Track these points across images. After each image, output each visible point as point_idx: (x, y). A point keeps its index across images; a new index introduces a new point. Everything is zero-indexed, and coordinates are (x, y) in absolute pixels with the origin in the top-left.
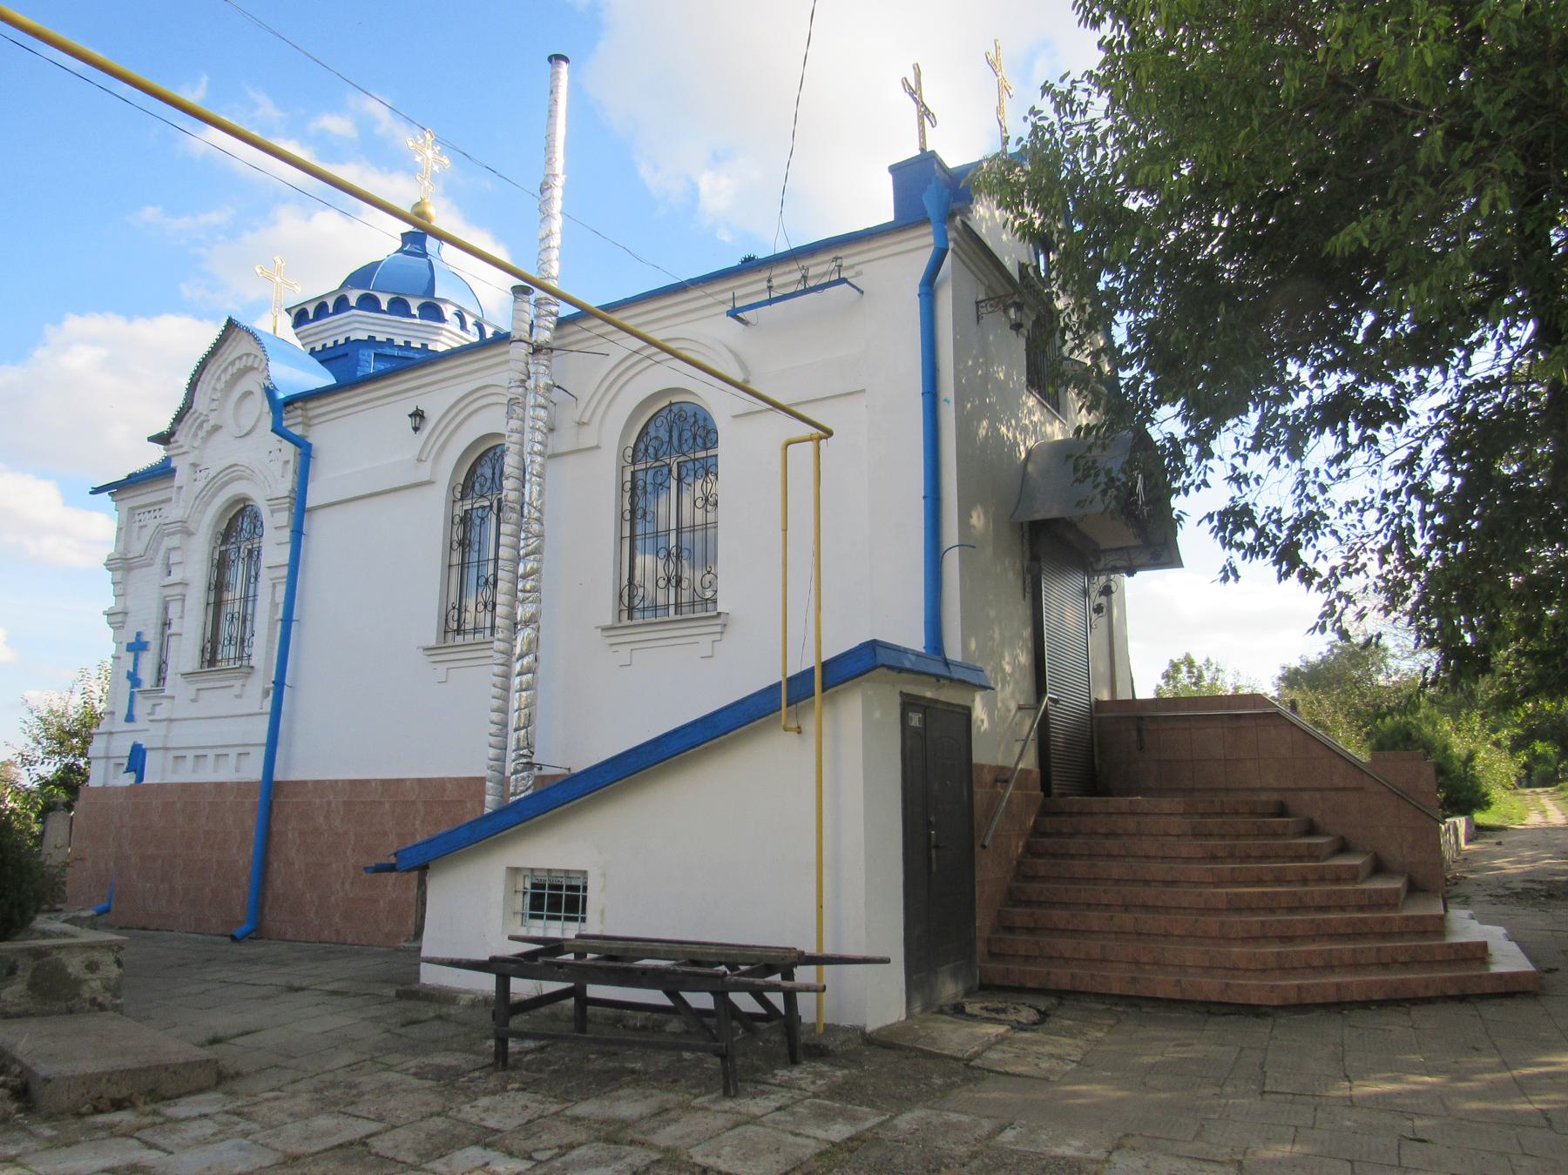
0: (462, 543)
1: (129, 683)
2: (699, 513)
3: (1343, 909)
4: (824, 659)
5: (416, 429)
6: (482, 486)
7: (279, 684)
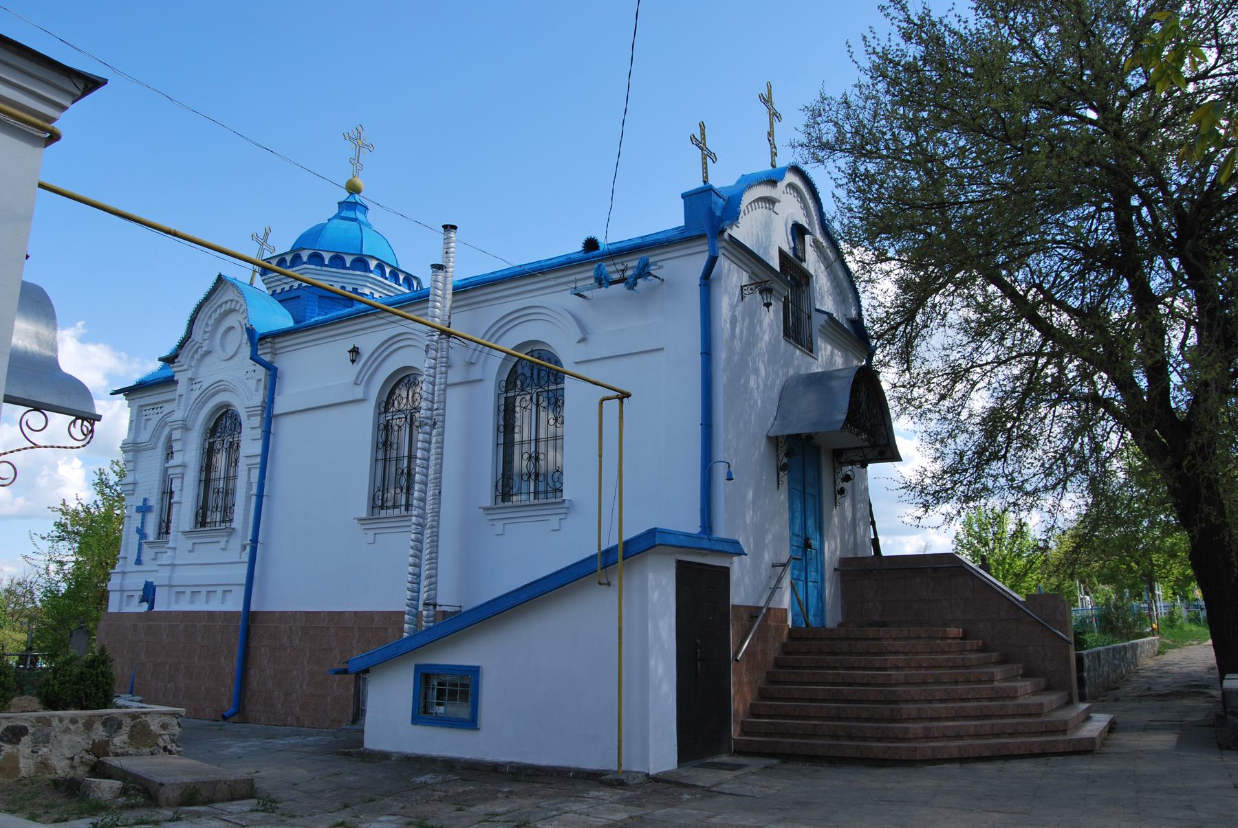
0: (385, 444)
1: (137, 537)
2: (552, 429)
3: (978, 700)
4: (624, 539)
5: (353, 361)
7: (255, 541)
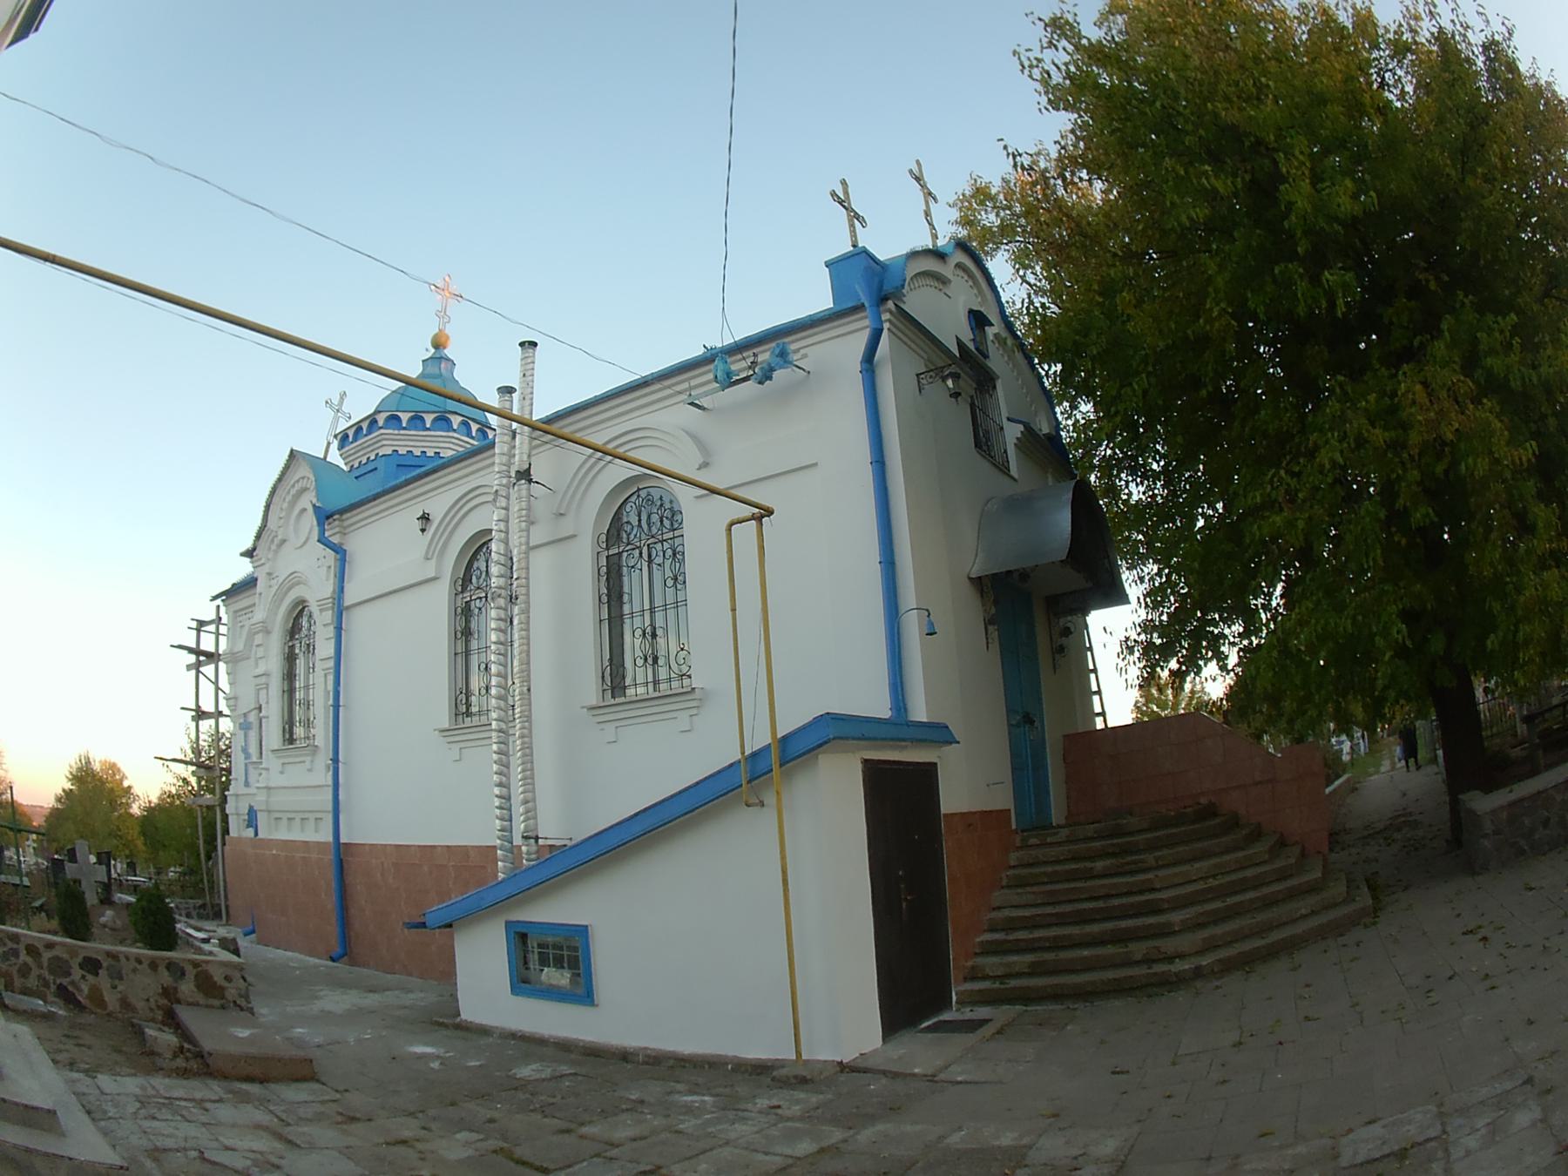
5: (423, 530)
6: (478, 578)
7: (336, 760)
